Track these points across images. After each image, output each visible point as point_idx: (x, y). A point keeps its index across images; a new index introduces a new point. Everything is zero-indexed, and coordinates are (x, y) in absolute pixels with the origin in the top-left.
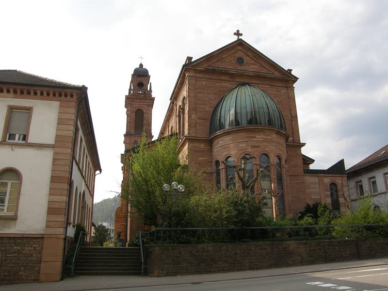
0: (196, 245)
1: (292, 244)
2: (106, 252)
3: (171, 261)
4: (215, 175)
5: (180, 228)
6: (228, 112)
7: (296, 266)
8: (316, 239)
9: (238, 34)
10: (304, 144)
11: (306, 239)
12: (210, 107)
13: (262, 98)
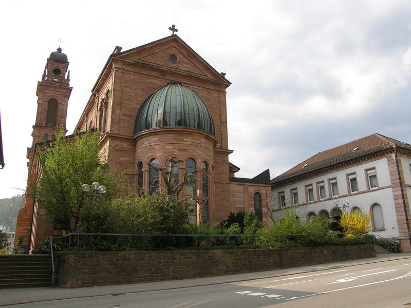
0: (116, 252)
1: (218, 252)
2: (7, 261)
3: (87, 271)
4: (136, 178)
5: (100, 233)
6: (156, 111)
7: (221, 275)
8: (241, 248)
9: (173, 29)
10: (231, 152)
11: (231, 248)
12: (137, 104)
13: (193, 99)
